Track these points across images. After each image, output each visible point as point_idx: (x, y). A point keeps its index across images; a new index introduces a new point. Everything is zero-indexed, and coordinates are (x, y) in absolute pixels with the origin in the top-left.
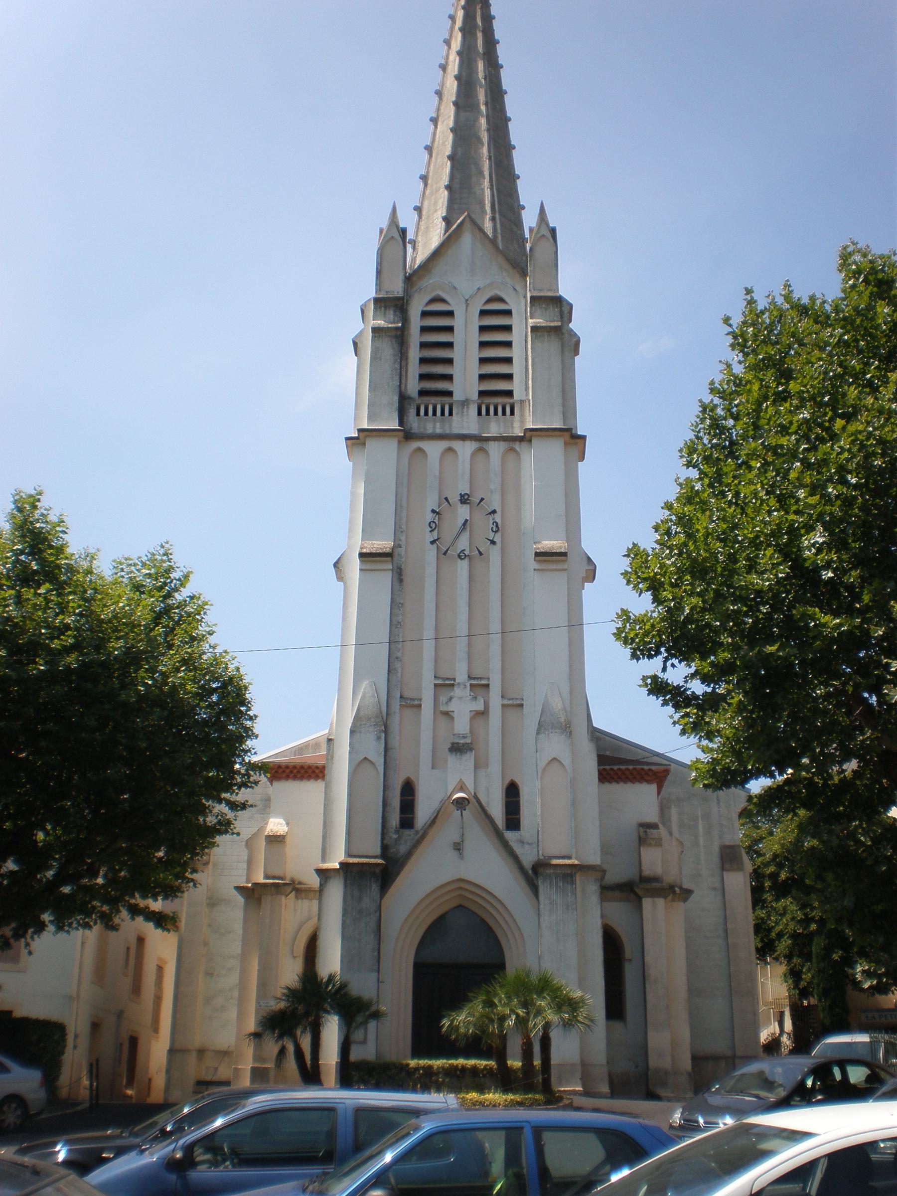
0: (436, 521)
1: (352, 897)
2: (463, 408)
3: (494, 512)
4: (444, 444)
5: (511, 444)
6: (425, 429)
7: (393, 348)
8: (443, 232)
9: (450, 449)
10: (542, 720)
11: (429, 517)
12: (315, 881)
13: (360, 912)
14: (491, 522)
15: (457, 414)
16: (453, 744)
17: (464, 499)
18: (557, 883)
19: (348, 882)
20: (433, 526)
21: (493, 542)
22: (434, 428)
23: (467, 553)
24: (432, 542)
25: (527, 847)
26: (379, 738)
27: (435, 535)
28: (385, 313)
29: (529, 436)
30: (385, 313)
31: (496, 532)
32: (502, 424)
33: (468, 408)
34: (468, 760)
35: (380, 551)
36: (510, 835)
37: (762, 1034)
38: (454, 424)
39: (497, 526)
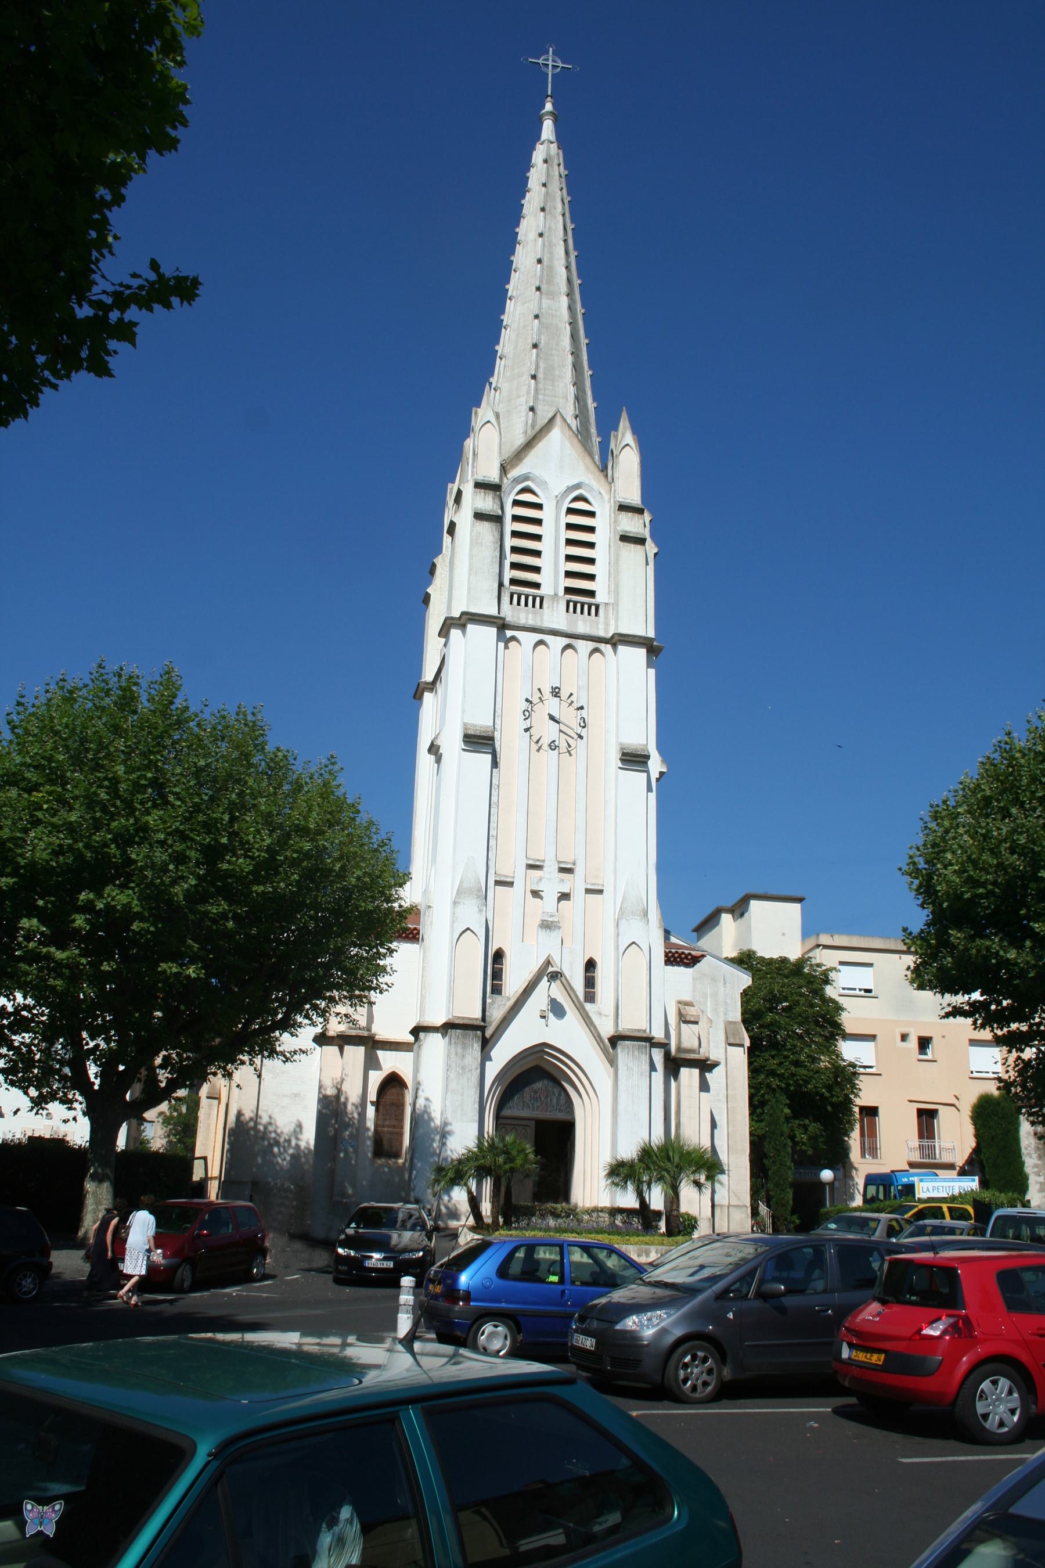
0: (530, 710)
1: (456, 1054)
2: (553, 603)
3: (582, 708)
4: (539, 637)
5: (598, 645)
6: (519, 618)
7: (494, 536)
8: (588, 460)
9: (541, 642)
10: (624, 906)
11: (525, 705)
12: (411, 1039)
13: (463, 1068)
14: (579, 717)
15: (548, 608)
16: (543, 921)
17: (556, 692)
18: (633, 1052)
19: (453, 1041)
20: (527, 714)
21: (581, 737)
22: (527, 619)
23: (557, 743)
24: (527, 730)
25: (604, 1018)
26: (481, 910)
27: (527, 724)
28: (484, 499)
29: (618, 640)
30: (484, 499)
31: (584, 727)
32: (588, 624)
33: (557, 603)
34: (555, 936)
35: (484, 734)
36: (588, 1006)
37: (632, 1257)
38: (545, 617)
39: (584, 722)
